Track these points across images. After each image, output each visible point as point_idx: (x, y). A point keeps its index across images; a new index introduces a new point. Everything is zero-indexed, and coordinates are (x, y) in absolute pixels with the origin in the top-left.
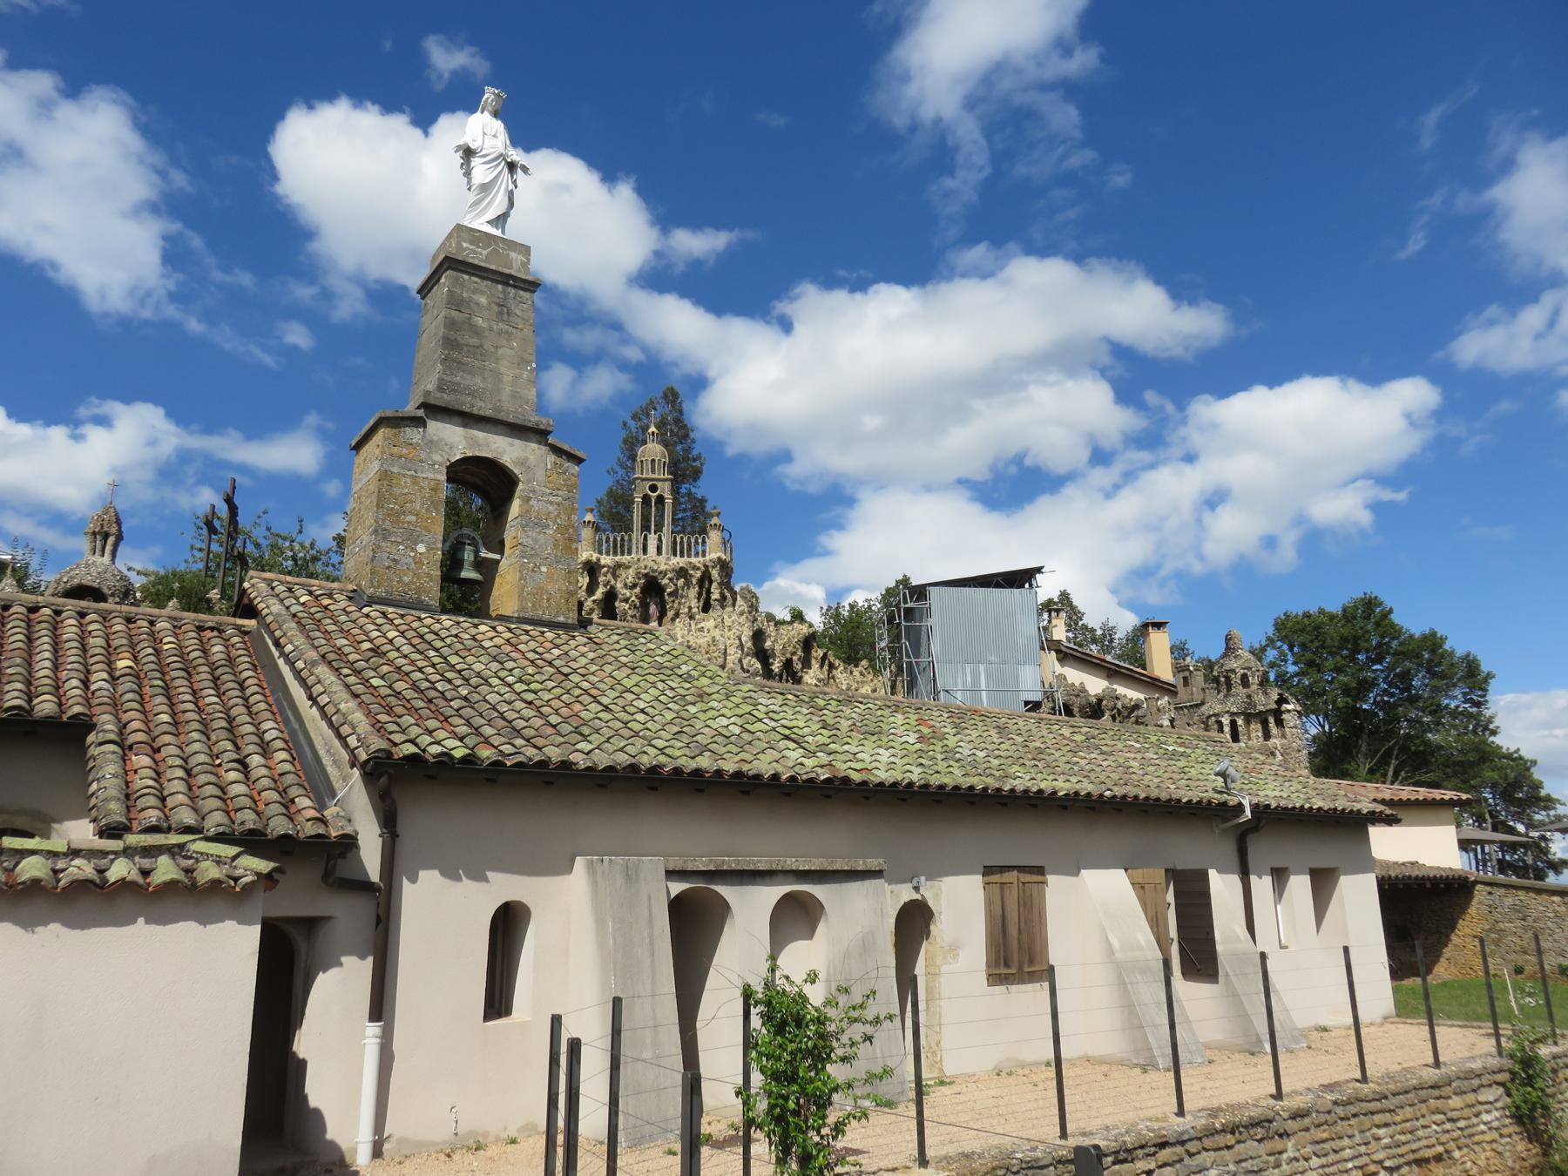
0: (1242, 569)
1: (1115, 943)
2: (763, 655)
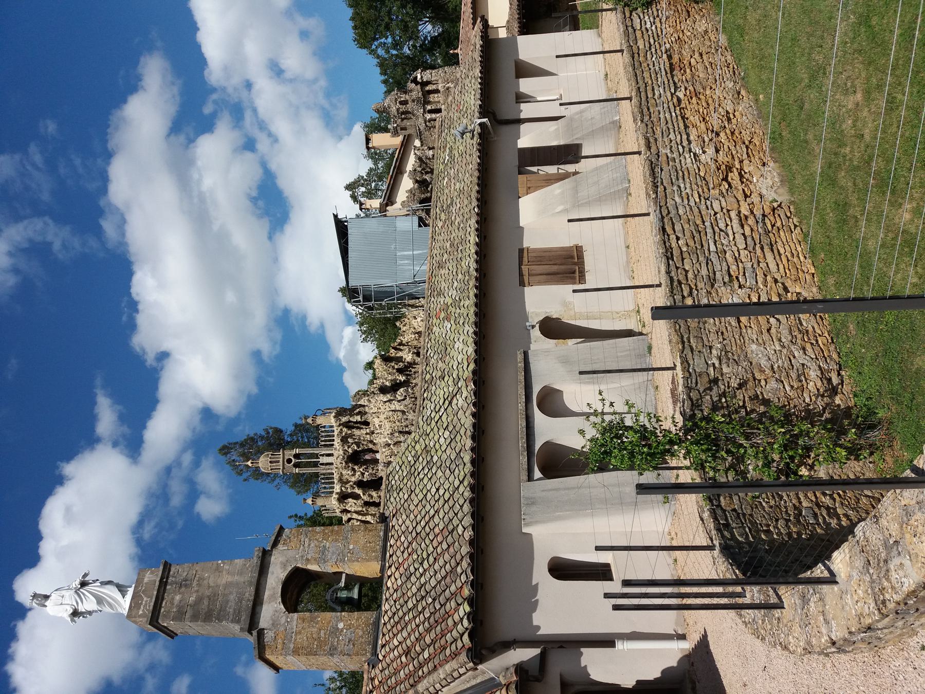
0: (323, 53)
1: (560, 208)
2: (395, 387)
